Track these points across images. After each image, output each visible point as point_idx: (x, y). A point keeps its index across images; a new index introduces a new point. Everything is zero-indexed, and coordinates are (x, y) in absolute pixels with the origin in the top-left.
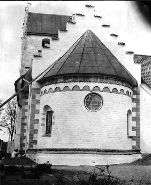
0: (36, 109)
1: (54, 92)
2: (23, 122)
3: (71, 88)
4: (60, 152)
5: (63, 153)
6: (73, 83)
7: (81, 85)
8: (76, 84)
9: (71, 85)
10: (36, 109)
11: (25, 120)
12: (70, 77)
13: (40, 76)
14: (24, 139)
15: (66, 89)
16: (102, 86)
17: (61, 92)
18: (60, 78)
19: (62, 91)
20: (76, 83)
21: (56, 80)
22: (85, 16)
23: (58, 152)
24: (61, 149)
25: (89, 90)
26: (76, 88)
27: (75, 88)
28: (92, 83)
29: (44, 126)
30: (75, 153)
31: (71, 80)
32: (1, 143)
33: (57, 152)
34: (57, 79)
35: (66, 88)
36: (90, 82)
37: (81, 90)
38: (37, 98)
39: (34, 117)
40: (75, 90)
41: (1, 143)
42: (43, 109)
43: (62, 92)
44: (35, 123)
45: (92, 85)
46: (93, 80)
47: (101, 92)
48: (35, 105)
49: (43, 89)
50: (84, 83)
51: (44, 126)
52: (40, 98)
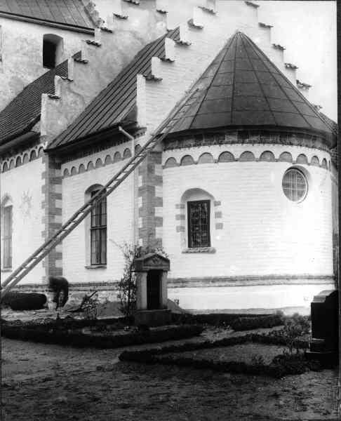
0: (157, 195)
1: (257, 161)
2: (52, 222)
3: (257, 156)
4: (242, 284)
5: (249, 286)
6: (261, 145)
7: (277, 150)
8: (224, 148)
9: (258, 149)
10: (157, 195)
11: (56, 217)
12: (254, 134)
13: (9, 143)
14: (57, 259)
15: (247, 156)
16: (309, 153)
17: (235, 163)
18: (230, 134)
19: (237, 161)
20: (266, 145)
21: (222, 137)
22: (191, 47)
23: (238, 283)
24: (244, 277)
25: (291, 161)
26: (186, 160)
27: (267, 155)
28: (295, 147)
29: (184, 231)
30: (274, 284)
31: (255, 138)
32: (340, 349)
33: (234, 284)
34: (223, 135)
35: (286, 156)
36: (291, 144)
37: (277, 161)
38: (157, 173)
39: (153, 213)
40: (265, 160)
41: (340, 349)
42: (182, 195)
43: (238, 163)
44: (156, 226)
45: (295, 151)
46: (296, 142)
47: (309, 164)
48: (154, 187)
49: (167, 155)
50: (281, 145)
51: (184, 231)
52: (162, 172)
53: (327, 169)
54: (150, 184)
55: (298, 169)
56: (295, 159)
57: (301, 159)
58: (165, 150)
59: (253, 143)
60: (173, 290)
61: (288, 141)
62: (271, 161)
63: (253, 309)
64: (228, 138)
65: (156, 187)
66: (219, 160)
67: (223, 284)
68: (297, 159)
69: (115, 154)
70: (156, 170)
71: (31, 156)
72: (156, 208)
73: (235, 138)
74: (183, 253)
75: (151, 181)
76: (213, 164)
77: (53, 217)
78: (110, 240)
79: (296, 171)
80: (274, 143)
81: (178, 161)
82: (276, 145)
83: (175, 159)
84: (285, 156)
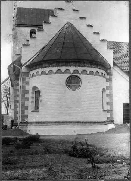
1: (55, 74)
6: (74, 67)
7: (63, 69)
9: (55, 69)
11: (17, 98)
15: (51, 72)
17: (46, 75)
25: (70, 73)
27: (59, 71)
31: (54, 65)
34: (42, 64)
35: (68, 71)
37: (63, 73)
40: (58, 73)
45: (72, 69)
47: (80, 74)
49: (31, 73)
53: (103, 77)
54: (23, 85)
55: (79, 78)
56: (72, 72)
57: (76, 72)
58: (30, 71)
59: (53, 66)
60: (30, 126)
61: (69, 65)
62: (60, 73)
63: (49, 136)
64: (45, 65)
65: (26, 86)
66: (41, 75)
67: (41, 124)
68: (73, 72)
69: (37, 72)
70: (26, 79)
71: (32, 75)
72: (26, 94)
73: (47, 65)
74: (32, 111)
75: (24, 84)
76: (39, 76)
77: (16, 98)
78: (122, 114)
79: (78, 78)
80: (62, 66)
81: (40, 73)
82: (63, 67)
83: (93, 72)
84: (66, 71)
